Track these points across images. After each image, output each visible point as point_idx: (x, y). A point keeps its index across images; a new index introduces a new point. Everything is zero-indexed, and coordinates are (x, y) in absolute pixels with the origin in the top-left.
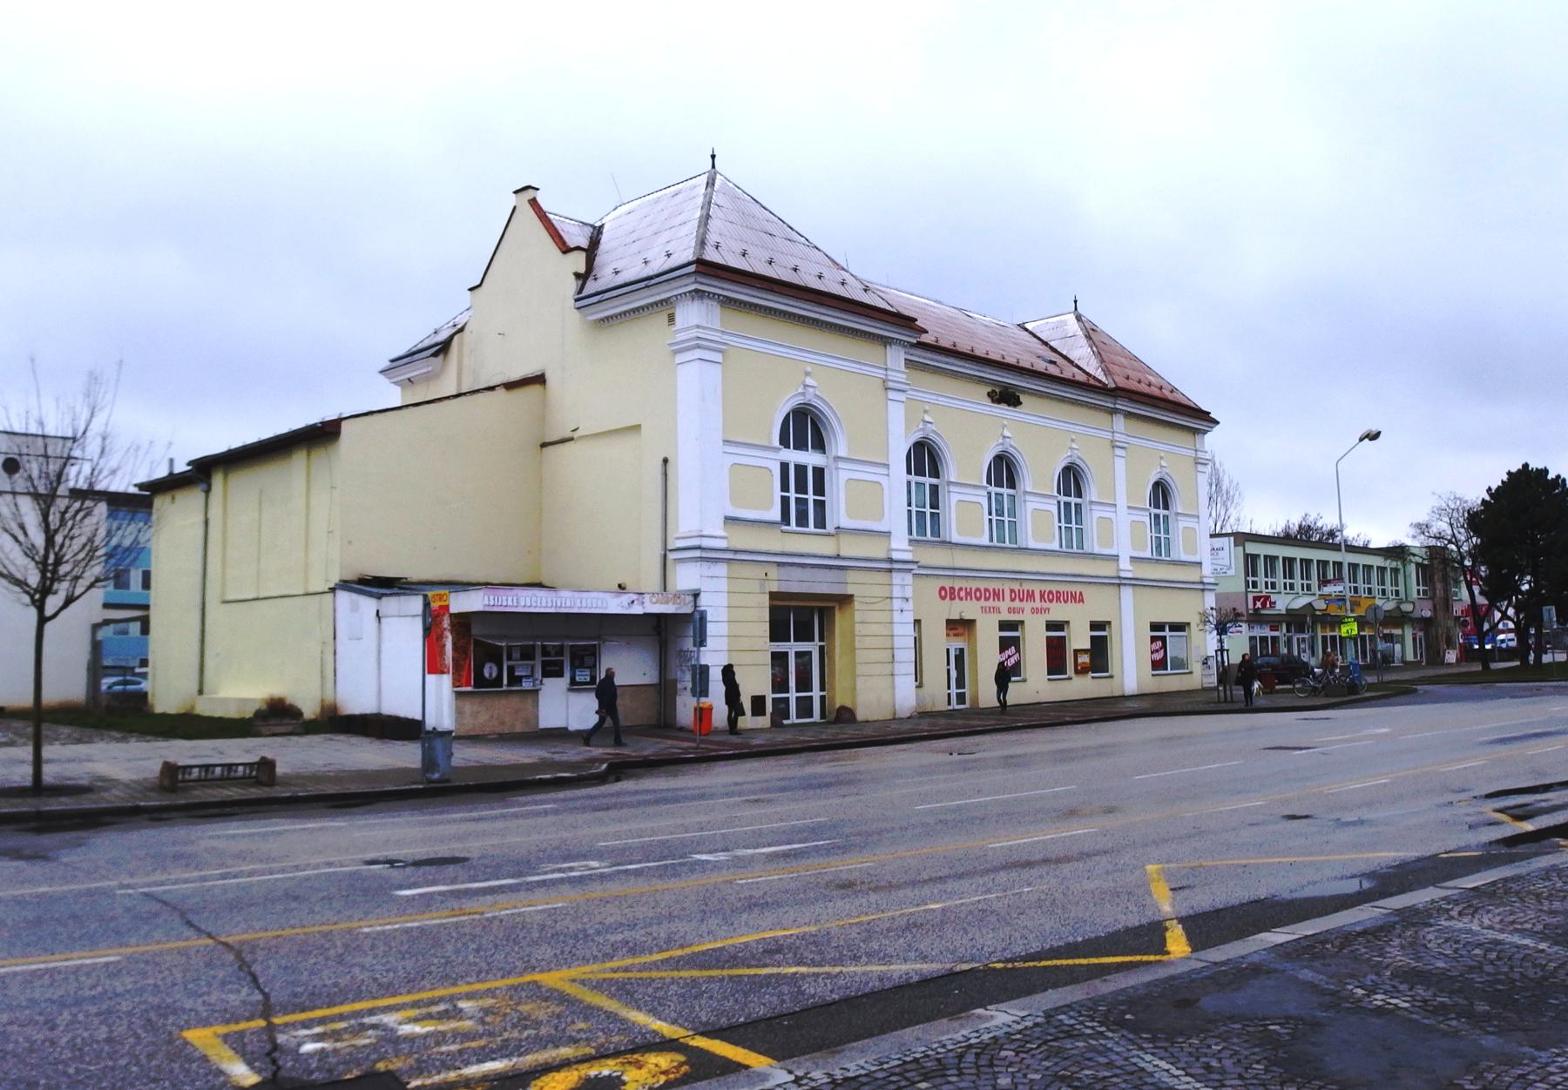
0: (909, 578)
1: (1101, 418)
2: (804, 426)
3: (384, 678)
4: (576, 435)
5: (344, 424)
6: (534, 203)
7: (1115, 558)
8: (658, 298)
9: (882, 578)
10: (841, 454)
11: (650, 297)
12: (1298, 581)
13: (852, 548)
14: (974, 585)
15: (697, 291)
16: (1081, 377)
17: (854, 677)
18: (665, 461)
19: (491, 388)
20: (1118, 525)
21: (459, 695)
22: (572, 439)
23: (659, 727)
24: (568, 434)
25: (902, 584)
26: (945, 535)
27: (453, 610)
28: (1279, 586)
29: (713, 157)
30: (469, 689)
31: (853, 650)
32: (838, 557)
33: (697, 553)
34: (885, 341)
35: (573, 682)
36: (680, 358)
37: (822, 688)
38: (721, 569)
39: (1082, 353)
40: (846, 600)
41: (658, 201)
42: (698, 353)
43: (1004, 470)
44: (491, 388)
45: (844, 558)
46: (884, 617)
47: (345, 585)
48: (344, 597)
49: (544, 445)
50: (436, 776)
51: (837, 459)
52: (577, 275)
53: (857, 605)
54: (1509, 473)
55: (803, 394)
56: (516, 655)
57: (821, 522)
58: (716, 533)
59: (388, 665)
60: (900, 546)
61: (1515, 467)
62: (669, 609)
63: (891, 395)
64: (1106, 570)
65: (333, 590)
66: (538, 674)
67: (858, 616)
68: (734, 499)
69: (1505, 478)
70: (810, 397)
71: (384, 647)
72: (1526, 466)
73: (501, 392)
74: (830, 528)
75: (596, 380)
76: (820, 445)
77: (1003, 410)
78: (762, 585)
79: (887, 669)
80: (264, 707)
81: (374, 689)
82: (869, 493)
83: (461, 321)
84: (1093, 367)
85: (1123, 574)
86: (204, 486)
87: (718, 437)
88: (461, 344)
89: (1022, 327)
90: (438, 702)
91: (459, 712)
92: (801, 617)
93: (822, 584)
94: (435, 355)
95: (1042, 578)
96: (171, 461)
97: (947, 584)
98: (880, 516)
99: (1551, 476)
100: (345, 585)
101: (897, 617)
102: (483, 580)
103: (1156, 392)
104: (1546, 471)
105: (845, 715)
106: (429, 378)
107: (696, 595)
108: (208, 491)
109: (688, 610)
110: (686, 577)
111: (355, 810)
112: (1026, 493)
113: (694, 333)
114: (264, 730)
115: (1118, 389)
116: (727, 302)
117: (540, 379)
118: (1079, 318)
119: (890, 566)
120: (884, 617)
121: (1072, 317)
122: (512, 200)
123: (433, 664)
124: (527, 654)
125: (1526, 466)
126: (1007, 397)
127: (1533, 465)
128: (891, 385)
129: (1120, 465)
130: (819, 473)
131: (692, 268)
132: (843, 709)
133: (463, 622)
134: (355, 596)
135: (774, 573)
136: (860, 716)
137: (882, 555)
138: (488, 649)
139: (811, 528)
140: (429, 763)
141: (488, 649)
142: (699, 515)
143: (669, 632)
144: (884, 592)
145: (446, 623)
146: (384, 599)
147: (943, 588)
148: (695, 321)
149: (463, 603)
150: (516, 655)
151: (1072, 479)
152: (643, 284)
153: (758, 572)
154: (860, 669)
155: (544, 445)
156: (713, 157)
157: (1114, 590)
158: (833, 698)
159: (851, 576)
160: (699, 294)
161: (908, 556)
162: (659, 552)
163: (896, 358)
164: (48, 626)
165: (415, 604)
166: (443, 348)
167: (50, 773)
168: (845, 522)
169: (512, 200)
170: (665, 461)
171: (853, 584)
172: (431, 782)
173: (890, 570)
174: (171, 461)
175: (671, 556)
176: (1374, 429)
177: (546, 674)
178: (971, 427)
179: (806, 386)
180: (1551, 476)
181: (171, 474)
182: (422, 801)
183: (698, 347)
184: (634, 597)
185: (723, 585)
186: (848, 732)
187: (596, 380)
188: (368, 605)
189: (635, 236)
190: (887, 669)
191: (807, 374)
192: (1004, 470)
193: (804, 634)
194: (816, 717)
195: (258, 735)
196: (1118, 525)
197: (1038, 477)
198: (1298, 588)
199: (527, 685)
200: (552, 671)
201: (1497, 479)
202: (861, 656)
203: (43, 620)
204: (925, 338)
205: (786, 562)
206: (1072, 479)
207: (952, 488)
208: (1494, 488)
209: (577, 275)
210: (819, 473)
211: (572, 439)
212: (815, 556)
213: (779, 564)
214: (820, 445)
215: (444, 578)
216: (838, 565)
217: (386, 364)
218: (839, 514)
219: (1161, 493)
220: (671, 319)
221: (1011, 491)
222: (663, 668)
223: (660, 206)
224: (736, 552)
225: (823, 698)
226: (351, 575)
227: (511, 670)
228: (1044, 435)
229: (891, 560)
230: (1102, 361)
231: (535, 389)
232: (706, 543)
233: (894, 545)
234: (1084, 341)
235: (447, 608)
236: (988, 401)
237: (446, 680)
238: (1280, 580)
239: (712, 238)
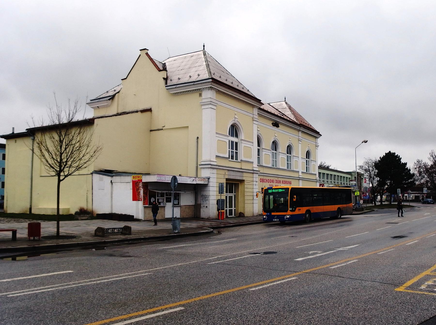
0: (257, 175)
1: (296, 132)
2: (234, 130)
3: (113, 202)
4: (164, 128)
5: (95, 120)
6: (147, 54)
7: (298, 172)
8: (197, 88)
9: (251, 175)
10: (243, 139)
11: (192, 88)
12: (329, 180)
13: (245, 166)
14: (267, 178)
15: (211, 87)
16: (288, 119)
17: (244, 203)
18: (198, 138)
19: (137, 112)
20: (299, 164)
21: (145, 207)
22: (162, 129)
23: (195, 218)
24: (161, 128)
25: (256, 178)
26: (261, 164)
27: (143, 181)
28: (325, 182)
29: (204, 46)
30: (147, 206)
31: (244, 196)
32: (241, 169)
33: (210, 166)
34: (253, 106)
35: (174, 204)
36: (203, 107)
37: (235, 207)
38: (215, 171)
39: (289, 114)
40: (242, 181)
41: (185, 58)
42: (210, 106)
43: (275, 145)
44: (137, 112)
45: (243, 169)
46: (251, 187)
47: (96, 172)
48: (96, 176)
49: (151, 131)
50: (177, 231)
51: (242, 140)
52: (164, 78)
53: (245, 183)
54: (386, 153)
55: (234, 120)
56: (159, 195)
57: (237, 159)
58: (215, 161)
59: (119, 198)
60: (255, 166)
61: (387, 152)
62: (202, 182)
63: (255, 122)
64: (295, 175)
65: (92, 174)
66: (165, 201)
67: (246, 186)
68: (218, 151)
69: (385, 155)
70: (236, 122)
71: (114, 192)
72: (390, 152)
73: (139, 113)
74: (239, 160)
75: (170, 112)
76: (237, 136)
77: (275, 128)
78: (224, 176)
79: (251, 202)
80: (78, 210)
81: (110, 205)
82: (248, 151)
83: (118, 89)
84: (292, 118)
85: (300, 177)
86: (32, 138)
87: (215, 131)
88: (118, 97)
89: (269, 104)
90: (137, 209)
91: (145, 213)
92: (233, 185)
93: (237, 177)
94: (109, 100)
95: (277, 176)
96: (13, 128)
97: (262, 177)
98: (251, 157)
99: (396, 155)
100: (96, 172)
101: (255, 187)
102: (134, 172)
103: (307, 126)
104: (395, 153)
105: (241, 215)
106: (107, 106)
107: (209, 179)
108: (34, 140)
109: (206, 183)
110: (205, 173)
111: (154, 243)
112: (279, 152)
113: (209, 100)
114: (79, 218)
115: (300, 124)
116: (218, 92)
117: (150, 110)
118: (286, 103)
119: (253, 172)
120: (251, 187)
121: (284, 103)
122: (139, 53)
123: (135, 198)
124: (162, 195)
125: (390, 152)
126: (276, 125)
127: (392, 152)
128: (255, 119)
129: (300, 145)
130: (236, 143)
131: (211, 80)
132: (240, 213)
133: (146, 185)
134: (101, 176)
135: (227, 173)
136: (246, 215)
137: (251, 169)
138: (154, 194)
139: (234, 160)
140: (175, 228)
141: (154, 194)
142: (208, 154)
143: (198, 190)
144: (251, 179)
145: (141, 185)
146: (114, 177)
147: (261, 179)
148: (210, 97)
149: (146, 179)
150: (159, 195)
151: (289, 149)
152: (192, 84)
153: (223, 172)
154: (246, 202)
155: (151, 131)
156: (204, 46)
157: (298, 181)
158: (238, 210)
159: (245, 174)
160: (211, 88)
161: (257, 169)
162: (195, 165)
163: (256, 111)
164: (61, 182)
165: (130, 179)
166: (112, 97)
167: (62, 231)
168: (243, 159)
169: (139, 53)
170: (198, 138)
171: (246, 177)
172: (175, 233)
173: (253, 173)
174: (13, 128)
175: (199, 167)
176: (366, 140)
177: (167, 201)
178: (270, 133)
179: (235, 118)
180: (396, 155)
181: (13, 133)
182: (180, 239)
183: (211, 104)
184: (194, 178)
185: (215, 176)
186: (241, 220)
187: (170, 112)
188: (107, 179)
189: (181, 68)
190: (251, 202)
191: (235, 114)
192: (275, 145)
193: (231, 192)
194: (233, 215)
195: (77, 220)
196: (299, 164)
197: (282, 148)
198: (329, 182)
199: (162, 205)
200: (168, 201)
201: (383, 154)
202: (246, 198)
203: (59, 181)
204: (262, 107)
205: (230, 170)
206: (289, 149)
207: (263, 150)
208: (382, 157)
209: (164, 78)
210: (236, 143)
211: (162, 129)
212: (236, 168)
213: (228, 170)
214: (237, 136)
215: (123, 171)
216: (241, 171)
217: (89, 101)
218: (242, 156)
219: (308, 154)
220: (200, 95)
221: (276, 152)
222: (196, 200)
223: (187, 59)
224: (219, 166)
225: (235, 210)
226: (97, 169)
227: (158, 200)
228: (285, 136)
229: (254, 170)
230: (295, 116)
231: (148, 113)
232: (212, 163)
233: (254, 166)
234: (289, 110)
235: (141, 180)
236: (272, 125)
237: (141, 203)
238: (326, 180)
239: (212, 72)
